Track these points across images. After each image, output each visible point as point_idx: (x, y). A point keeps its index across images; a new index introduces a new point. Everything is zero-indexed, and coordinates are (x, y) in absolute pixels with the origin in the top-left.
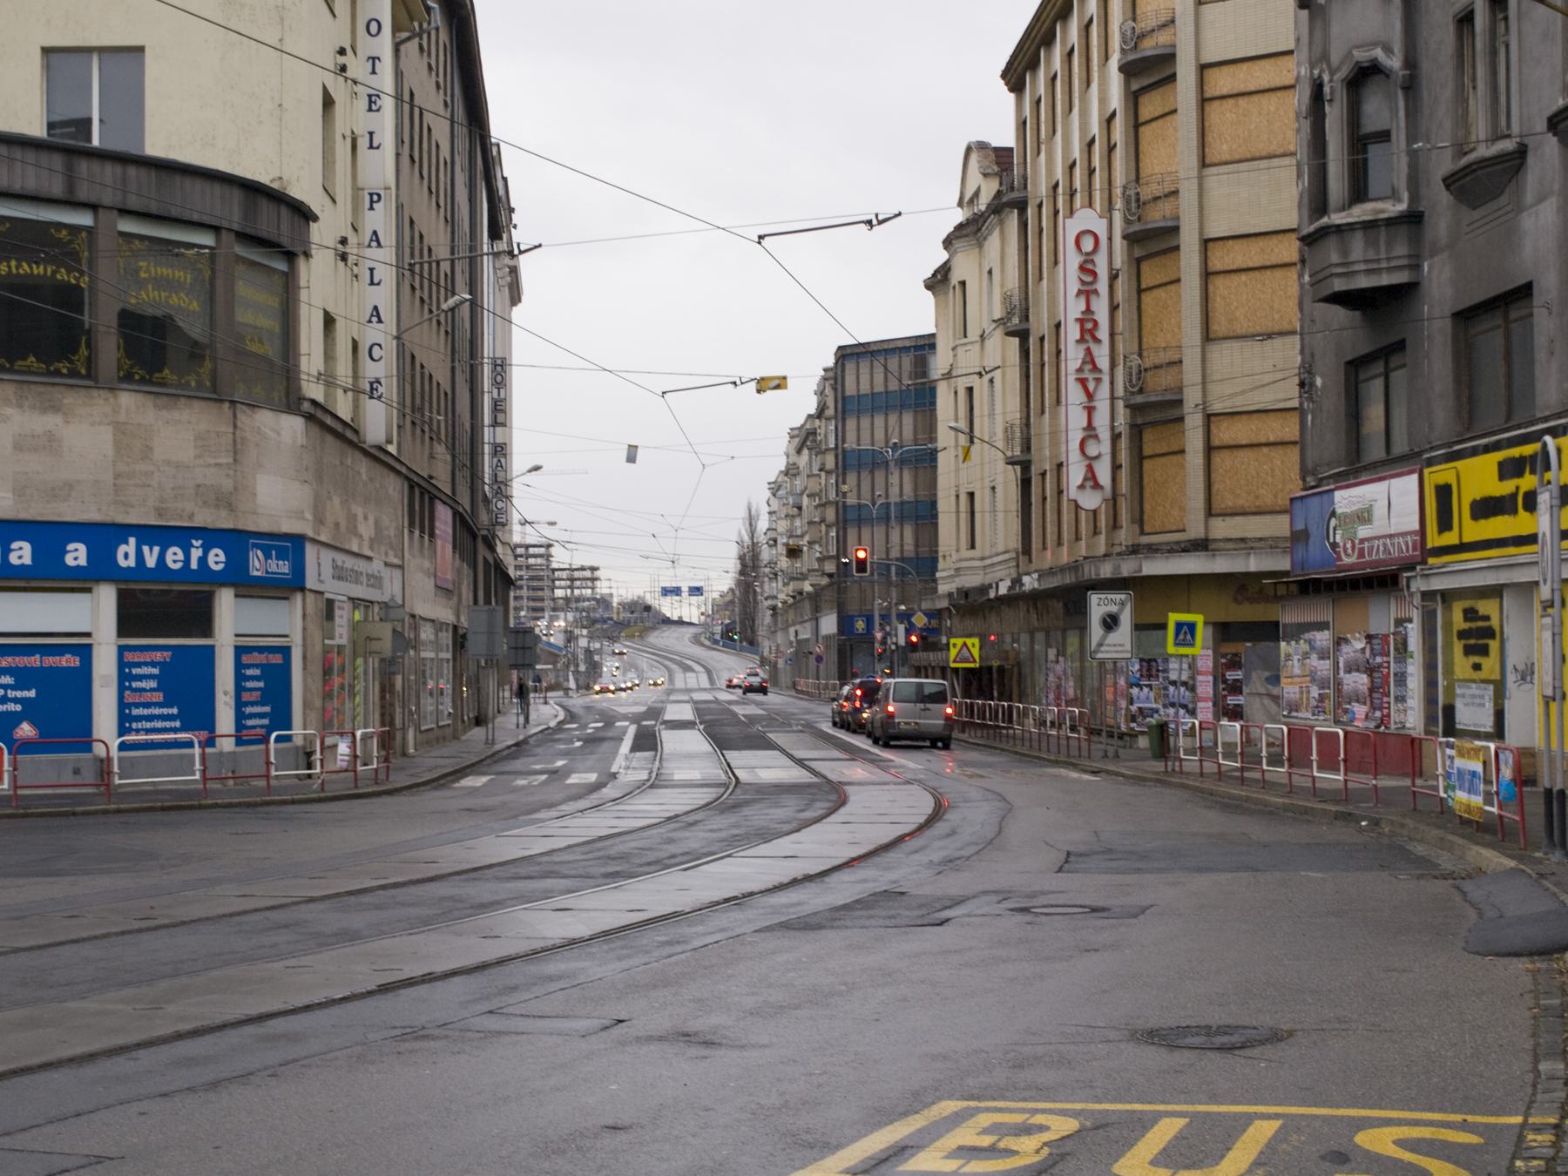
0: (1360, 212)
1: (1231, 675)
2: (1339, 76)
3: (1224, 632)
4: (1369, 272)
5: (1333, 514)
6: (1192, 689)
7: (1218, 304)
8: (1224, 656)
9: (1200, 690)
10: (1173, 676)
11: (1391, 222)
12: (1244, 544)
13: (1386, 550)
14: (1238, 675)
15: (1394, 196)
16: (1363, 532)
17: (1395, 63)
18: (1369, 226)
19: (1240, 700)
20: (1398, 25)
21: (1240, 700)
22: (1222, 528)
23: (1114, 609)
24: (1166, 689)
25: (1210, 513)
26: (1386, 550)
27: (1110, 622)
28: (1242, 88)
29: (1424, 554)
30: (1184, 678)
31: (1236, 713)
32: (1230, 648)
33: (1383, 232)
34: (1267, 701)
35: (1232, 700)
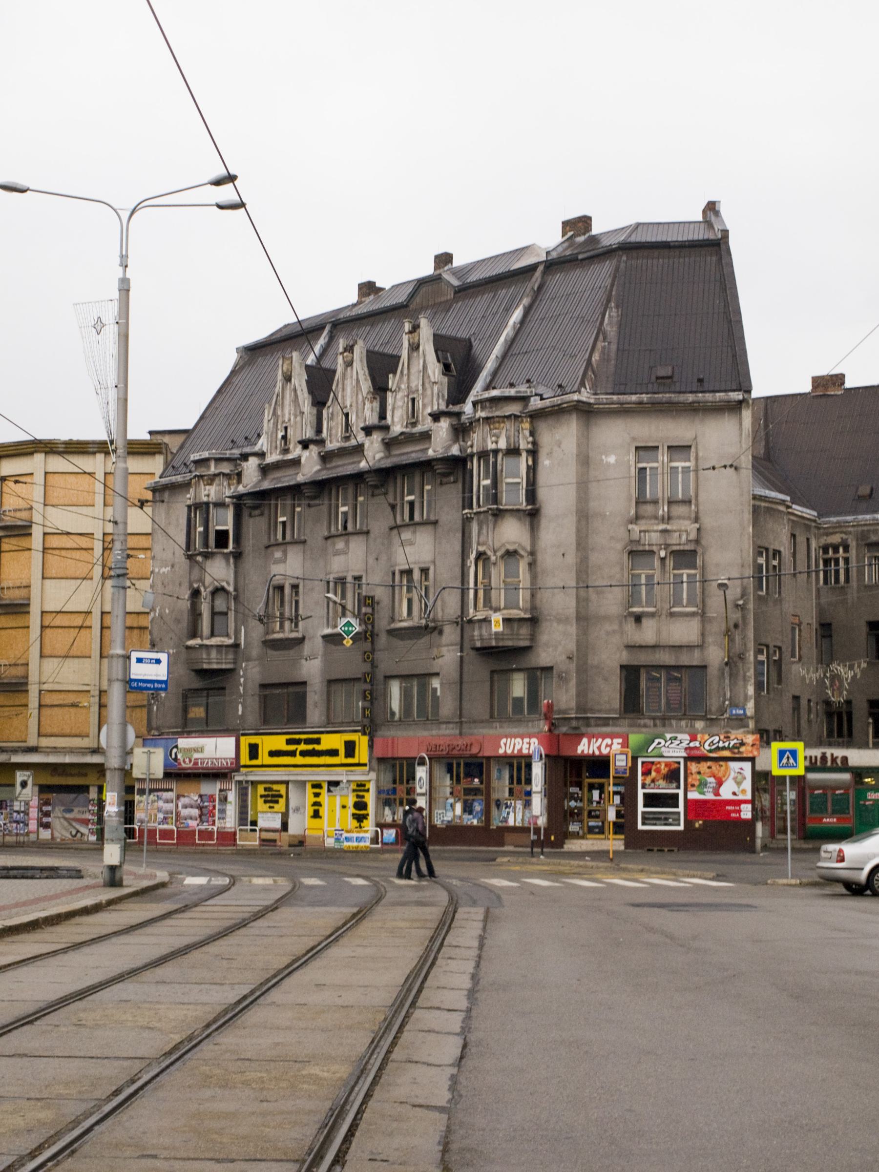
0: (214, 641)
1: (45, 808)
2: (208, 590)
3: (44, 789)
4: (218, 663)
5: (176, 747)
6: (28, 814)
7: (47, 640)
8: (42, 799)
9: (31, 815)
10: (16, 808)
11: (227, 646)
12: (55, 750)
13: (212, 763)
14: (49, 808)
15: (228, 635)
16: (196, 755)
17: (231, 589)
18: (219, 647)
19: (49, 819)
20: (232, 575)
21: (49, 819)
22: (45, 742)
23: (25, 778)
24: (11, 814)
25: (39, 735)
26: (212, 763)
27: (24, 784)
28: (63, 546)
29: (237, 766)
30: (23, 809)
31: (47, 826)
32: (45, 796)
33: (224, 649)
34: (62, 820)
35: (45, 820)
